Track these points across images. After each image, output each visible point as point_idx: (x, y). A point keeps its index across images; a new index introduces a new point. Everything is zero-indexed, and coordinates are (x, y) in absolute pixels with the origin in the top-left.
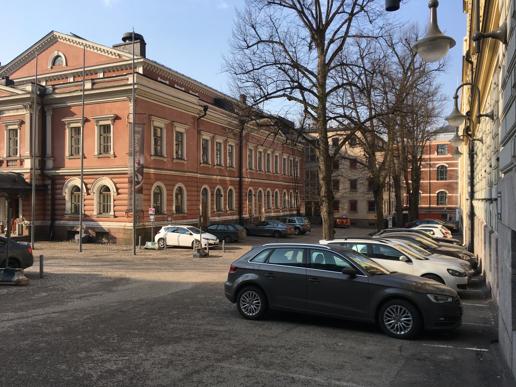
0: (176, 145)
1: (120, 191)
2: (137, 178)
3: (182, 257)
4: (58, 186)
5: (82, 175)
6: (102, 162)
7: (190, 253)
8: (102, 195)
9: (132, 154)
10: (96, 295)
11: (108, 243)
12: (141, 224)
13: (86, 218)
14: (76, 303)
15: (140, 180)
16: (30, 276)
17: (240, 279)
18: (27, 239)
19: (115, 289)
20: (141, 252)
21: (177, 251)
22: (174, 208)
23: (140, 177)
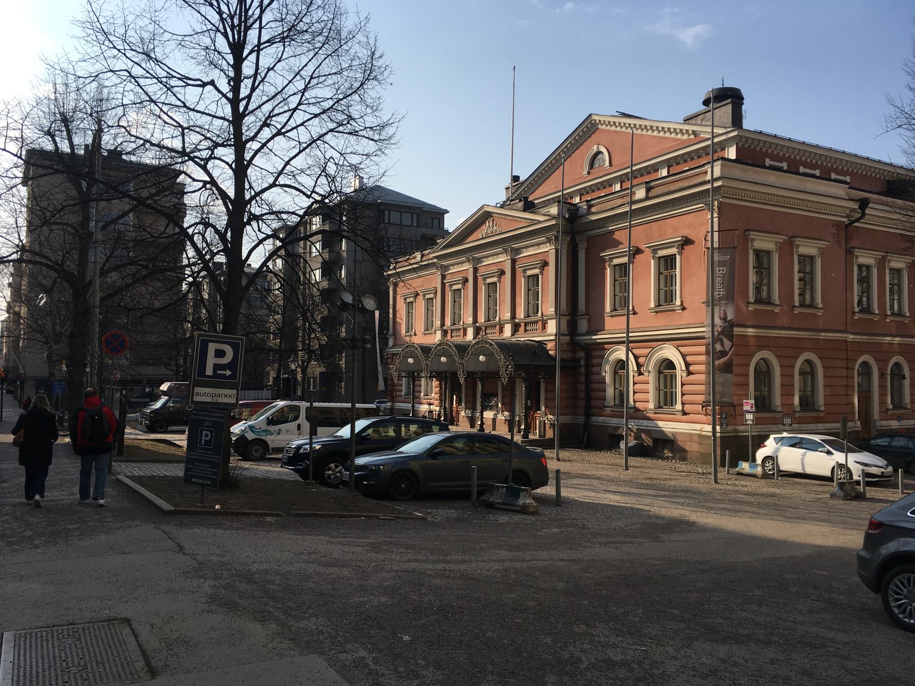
0: (800, 280)
1: (692, 368)
2: (722, 344)
3: (807, 496)
4: (595, 361)
5: (628, 343)
6: (661, 320)
7: (826, 489)
8: (662, 376)
9: (711, 303)
10: (631, 542)
11: (673, 458)
12: (730, 428)
13: (637, 414)
14: (597, 550)
15: (727, 348)
16: (542, 500)
17: (892, 547)
18: (547, 444)
19: (665, 537)
20: (729, 479)
21: (800, 484)
22: (796, 400)
23: (727, 344)
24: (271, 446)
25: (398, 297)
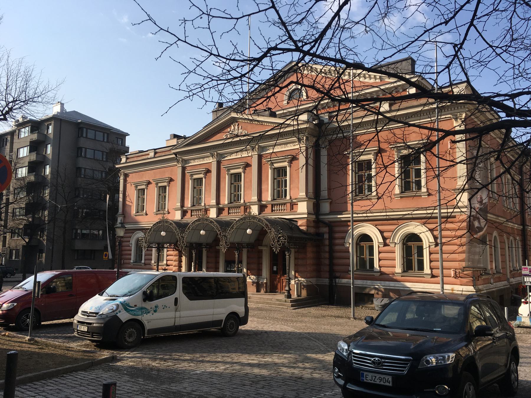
2: (479, 222)
8: (358, 246)
13: (383, 276)
24: (148, 326)
25: (128, 185)
